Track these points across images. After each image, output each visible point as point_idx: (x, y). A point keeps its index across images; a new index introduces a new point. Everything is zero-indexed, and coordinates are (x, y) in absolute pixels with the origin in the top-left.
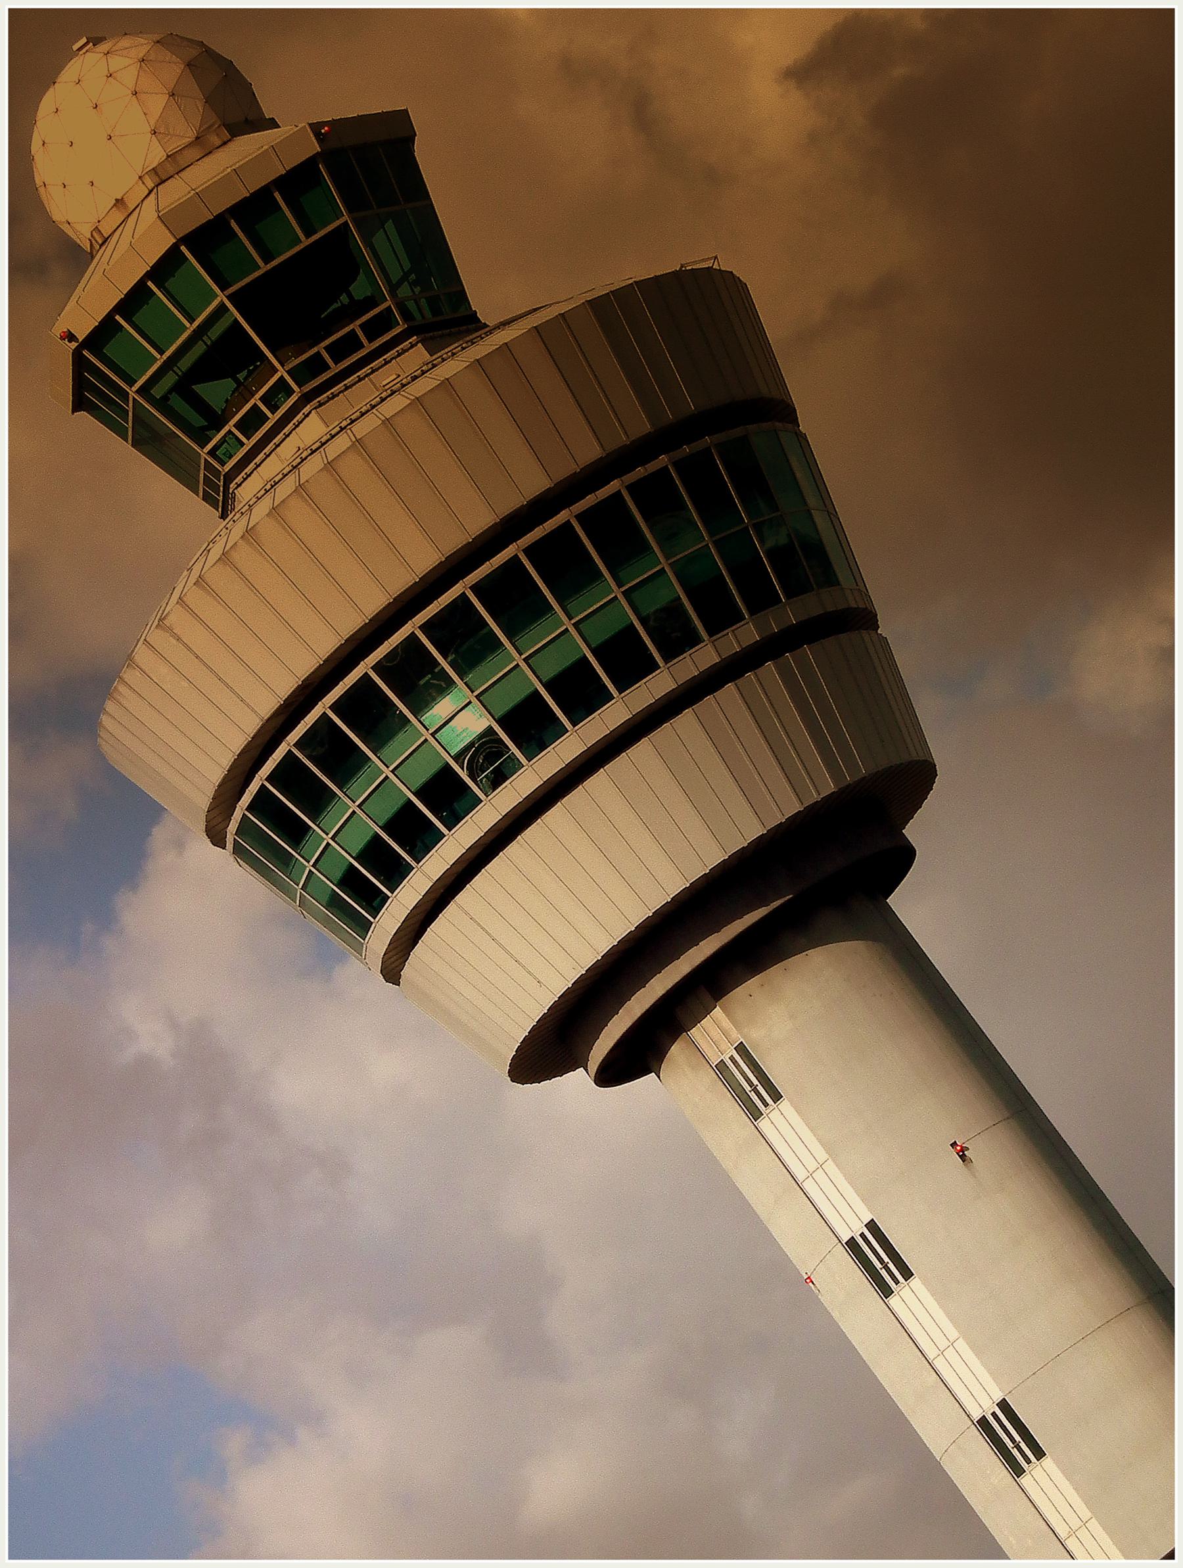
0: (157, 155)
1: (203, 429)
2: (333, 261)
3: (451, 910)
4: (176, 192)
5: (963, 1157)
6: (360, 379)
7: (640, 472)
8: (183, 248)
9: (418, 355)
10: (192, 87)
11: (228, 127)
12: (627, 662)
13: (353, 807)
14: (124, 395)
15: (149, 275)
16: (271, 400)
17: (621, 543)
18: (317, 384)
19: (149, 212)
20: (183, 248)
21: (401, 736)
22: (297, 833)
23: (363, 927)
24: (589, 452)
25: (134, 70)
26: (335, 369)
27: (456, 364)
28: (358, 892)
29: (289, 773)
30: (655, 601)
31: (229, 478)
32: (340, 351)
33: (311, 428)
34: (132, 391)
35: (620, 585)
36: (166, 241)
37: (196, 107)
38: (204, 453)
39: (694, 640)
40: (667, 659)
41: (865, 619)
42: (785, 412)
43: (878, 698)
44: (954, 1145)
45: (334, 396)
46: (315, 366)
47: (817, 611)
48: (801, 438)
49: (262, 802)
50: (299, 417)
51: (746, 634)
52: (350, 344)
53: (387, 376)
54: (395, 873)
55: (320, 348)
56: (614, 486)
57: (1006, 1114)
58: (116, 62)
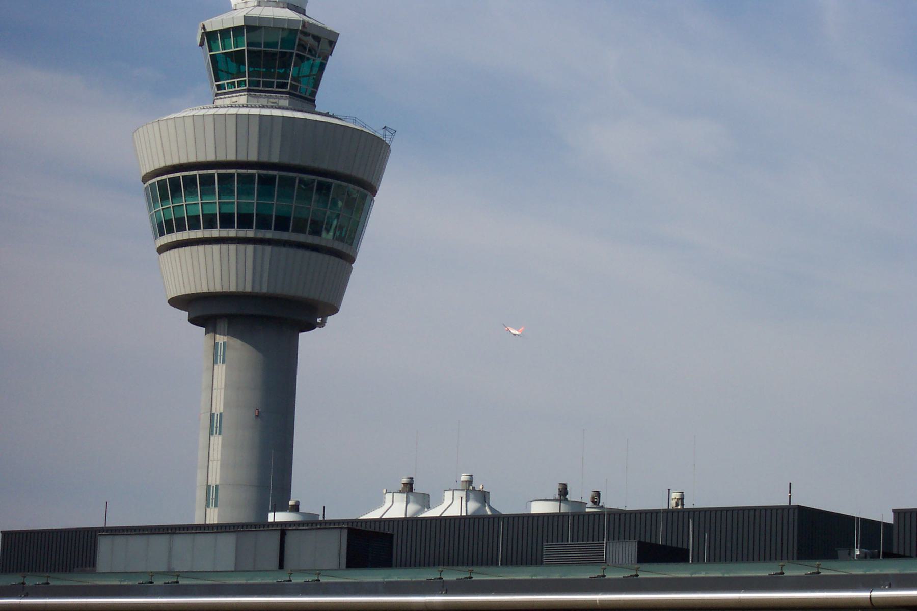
1: (285, 72)
2: (285, 61)
3: (188, 249)
12: (227, 221)
13: (171, 205)
15: (220, 31)
17: (245, 191)
22: (164, 198)
23: (162, 234)
28: (165, 227)
29: (175, 182)
30: (226, 210)
32: (266, 84)
39: (269, 228)
40: (275, 229)
41: (352, 260)
42: (374, 191)
47: (175, 240)
48: (373, 199)
52: (270, 84)
54: (181, 228)
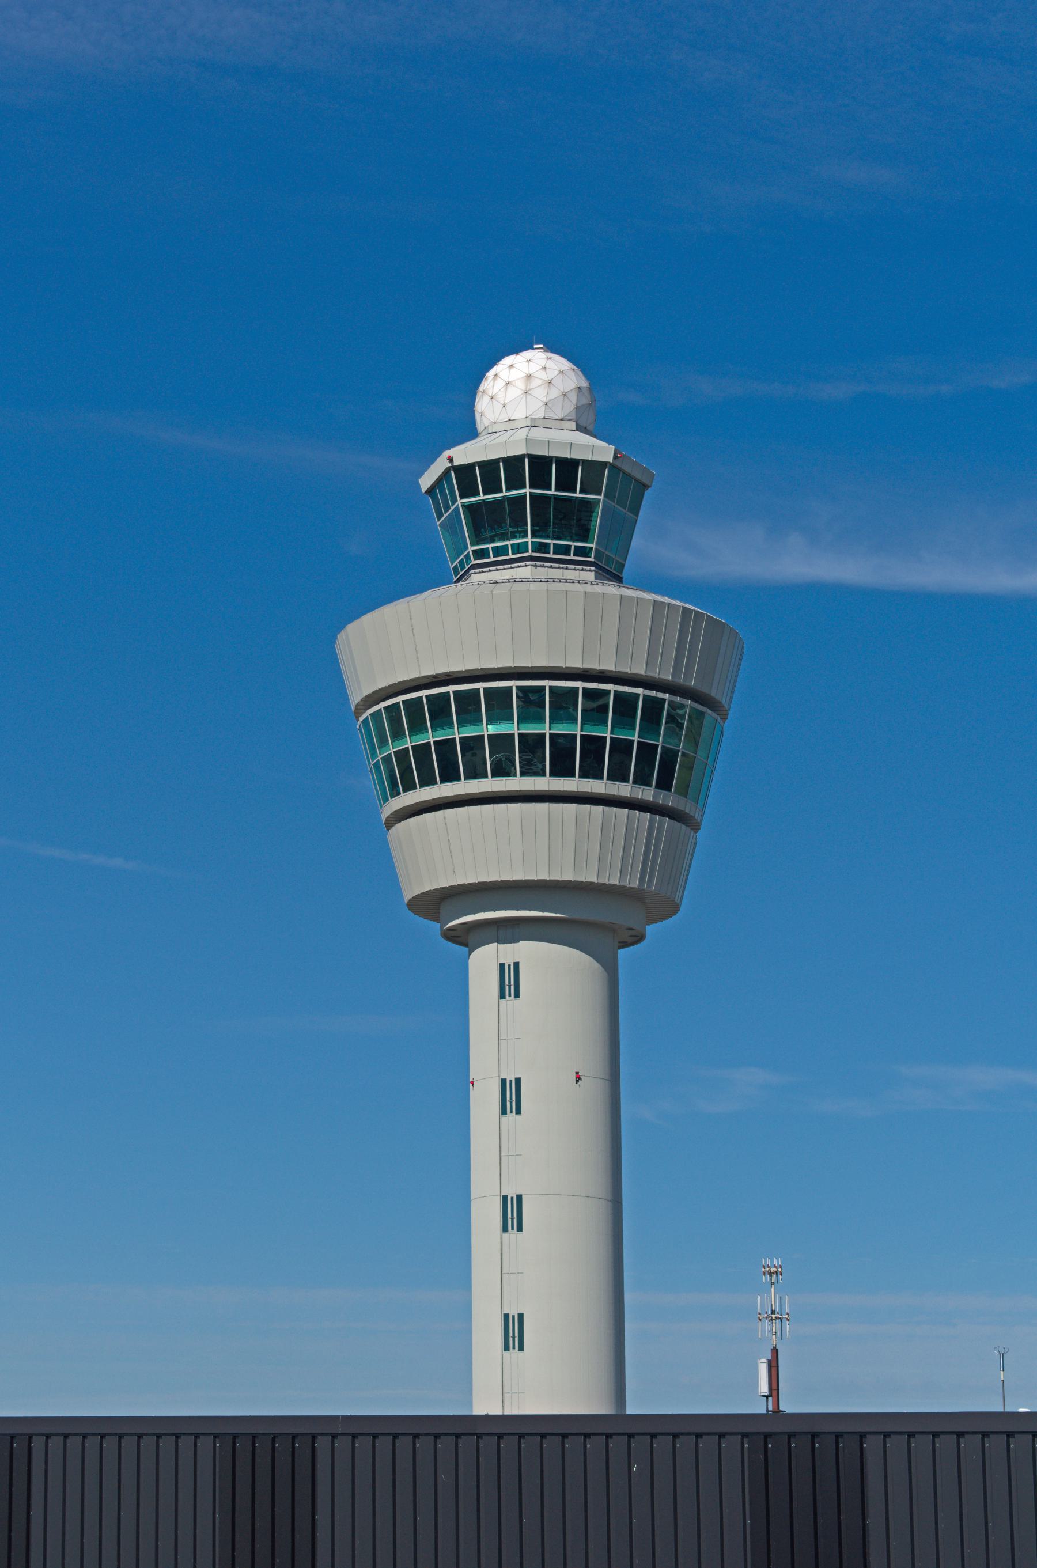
0: (541, 414)
4: (537, 434)
5: (577, 1082)
6: (559, 568)
7: (653, 693)
8: (527, 460)
9: (590, 576)
10: (573, 397)
11: (577, 425)
14: (454, 501)
16: (558, 549)
18: (540, 556)
19: (522, 434)
20: (527, 460)
21: (476, 727)
24: (639, 669)
25: (556, 372)
26: (572, 557)
27: (611, 589)
29: (414, 706)
31: (473, 567)
32: (558, 549)
33: (525, 571)
34: (459, 502)
35: (612, 733)
36: (521, 450)
37: (570, 407)
38: (470, 549)
39: (624, 779)
43: (671, 864)
44: (577, 1073)
45: (543, 566)
46: (543, 548)
49: (392, 710)
50: (523, 564)
51: (647, 794)
53: (570, 574)
55: (573, 544)
56: (666, 696)
57: (607, 1077)
58: (550, 364)
